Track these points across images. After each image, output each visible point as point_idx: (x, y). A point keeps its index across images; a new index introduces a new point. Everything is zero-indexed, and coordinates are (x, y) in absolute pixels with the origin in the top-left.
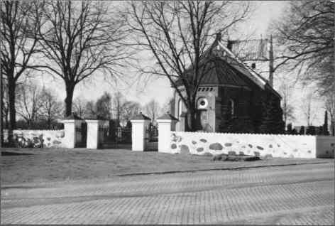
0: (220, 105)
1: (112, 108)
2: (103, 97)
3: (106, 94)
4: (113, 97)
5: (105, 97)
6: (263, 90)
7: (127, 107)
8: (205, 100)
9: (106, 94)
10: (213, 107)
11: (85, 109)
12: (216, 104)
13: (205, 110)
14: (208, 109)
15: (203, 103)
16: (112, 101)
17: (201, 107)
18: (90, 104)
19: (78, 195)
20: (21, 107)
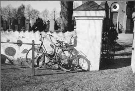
0: (129, 8)
1: (26, 13)
2: (21, 7)
3: (22, 5)
4: (26, 7)
5: (22, 7)
6: (33, 30)
7: (33, 12)
8: (117, 5)
9: (22, 5)
10: (125, 10)
11: (13, 13)
12: (127, 7)
13: (117, 12)
14: (119, 11)
15: (115, 7)
16: (26, 9)
17: (114, 10)
18: (15, 10)
19: (75, 73)
20: (41, 71)
